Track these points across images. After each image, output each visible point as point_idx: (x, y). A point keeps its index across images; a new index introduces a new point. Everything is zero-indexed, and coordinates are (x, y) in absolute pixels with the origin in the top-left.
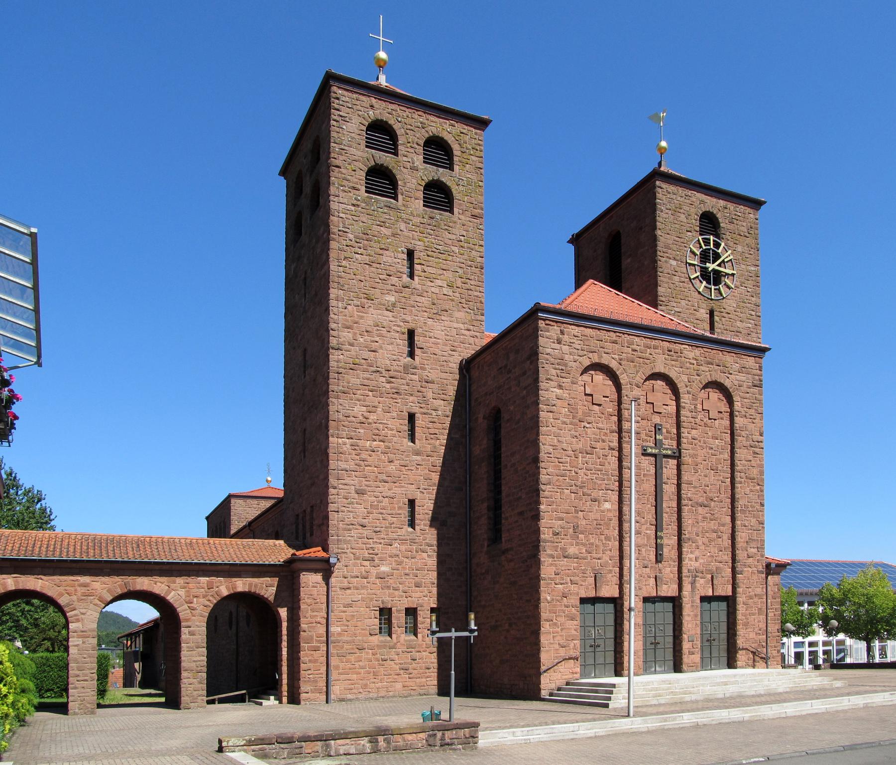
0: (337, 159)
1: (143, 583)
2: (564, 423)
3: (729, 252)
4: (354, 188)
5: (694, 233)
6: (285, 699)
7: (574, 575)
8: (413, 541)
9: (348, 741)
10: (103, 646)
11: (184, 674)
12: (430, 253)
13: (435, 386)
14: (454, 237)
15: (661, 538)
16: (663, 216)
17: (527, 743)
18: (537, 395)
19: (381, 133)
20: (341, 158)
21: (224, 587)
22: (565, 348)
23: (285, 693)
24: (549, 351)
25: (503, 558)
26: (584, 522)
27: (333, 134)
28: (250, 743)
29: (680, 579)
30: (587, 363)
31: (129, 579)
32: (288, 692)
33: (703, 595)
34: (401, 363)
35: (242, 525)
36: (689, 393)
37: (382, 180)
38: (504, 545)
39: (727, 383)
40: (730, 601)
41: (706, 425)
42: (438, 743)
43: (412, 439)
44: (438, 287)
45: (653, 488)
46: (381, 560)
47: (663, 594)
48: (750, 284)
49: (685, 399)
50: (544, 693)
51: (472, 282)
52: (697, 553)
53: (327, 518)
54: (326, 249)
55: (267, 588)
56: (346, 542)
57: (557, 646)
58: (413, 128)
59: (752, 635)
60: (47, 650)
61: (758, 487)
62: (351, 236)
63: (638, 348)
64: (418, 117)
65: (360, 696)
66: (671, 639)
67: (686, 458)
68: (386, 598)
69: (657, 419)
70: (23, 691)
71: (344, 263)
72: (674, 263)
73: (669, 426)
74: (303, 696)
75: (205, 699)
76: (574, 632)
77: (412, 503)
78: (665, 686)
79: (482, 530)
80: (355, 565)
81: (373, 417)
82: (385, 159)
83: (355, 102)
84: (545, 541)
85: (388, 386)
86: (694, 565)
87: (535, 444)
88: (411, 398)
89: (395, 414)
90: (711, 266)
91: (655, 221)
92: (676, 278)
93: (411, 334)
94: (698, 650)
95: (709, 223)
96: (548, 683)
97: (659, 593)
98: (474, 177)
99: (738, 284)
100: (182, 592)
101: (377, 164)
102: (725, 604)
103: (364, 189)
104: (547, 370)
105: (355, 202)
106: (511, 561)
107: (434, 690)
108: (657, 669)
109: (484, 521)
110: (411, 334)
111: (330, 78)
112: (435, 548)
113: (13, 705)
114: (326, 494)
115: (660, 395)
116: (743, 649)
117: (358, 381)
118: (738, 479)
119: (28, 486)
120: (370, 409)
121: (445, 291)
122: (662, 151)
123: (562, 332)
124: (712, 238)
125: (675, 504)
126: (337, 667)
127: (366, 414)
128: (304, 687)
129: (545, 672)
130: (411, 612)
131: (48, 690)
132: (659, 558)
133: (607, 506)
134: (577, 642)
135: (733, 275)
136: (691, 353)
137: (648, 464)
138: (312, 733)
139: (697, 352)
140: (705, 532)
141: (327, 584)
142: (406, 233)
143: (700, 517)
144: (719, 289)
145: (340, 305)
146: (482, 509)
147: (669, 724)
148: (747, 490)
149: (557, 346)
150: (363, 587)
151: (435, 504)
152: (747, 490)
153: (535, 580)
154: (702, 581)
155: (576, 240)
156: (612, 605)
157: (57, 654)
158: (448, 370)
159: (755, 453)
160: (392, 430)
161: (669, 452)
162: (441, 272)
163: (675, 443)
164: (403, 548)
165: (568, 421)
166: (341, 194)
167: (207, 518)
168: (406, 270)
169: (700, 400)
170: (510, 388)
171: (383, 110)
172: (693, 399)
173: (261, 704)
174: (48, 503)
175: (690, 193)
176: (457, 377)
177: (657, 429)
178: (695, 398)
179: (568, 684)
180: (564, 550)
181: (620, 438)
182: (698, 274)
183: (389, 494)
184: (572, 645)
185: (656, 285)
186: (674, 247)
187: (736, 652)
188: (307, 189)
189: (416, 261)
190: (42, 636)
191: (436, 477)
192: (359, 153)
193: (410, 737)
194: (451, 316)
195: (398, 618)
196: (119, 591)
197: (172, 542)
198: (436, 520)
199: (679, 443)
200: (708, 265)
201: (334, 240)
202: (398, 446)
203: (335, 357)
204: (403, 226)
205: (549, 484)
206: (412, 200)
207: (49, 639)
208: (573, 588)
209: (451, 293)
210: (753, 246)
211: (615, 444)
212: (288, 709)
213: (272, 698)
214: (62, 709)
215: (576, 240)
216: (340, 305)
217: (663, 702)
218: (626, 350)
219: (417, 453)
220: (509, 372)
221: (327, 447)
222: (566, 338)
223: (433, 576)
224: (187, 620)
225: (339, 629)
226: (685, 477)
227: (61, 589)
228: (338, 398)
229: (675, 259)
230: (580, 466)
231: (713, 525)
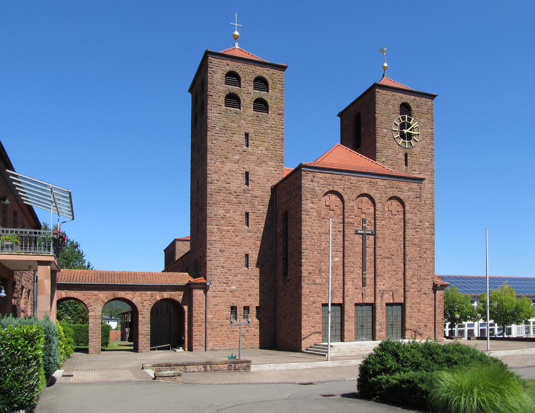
0: (211, 91)
1: (122, 294)
2: (315, 220)
3: (416, 123)
4: (219, 105)
5: (397, 114)
6: (186, 349)
8: (247, 274)
9: (194, 366)
10: (113, 318)
11: (140, 336)
12: (256, 134)
13: (259, 199)
14: (269, 125)
15: (365, 274)
16: (380, 107)
17: (275, 370)
18: (301, 207)
19: (233, 77)
20: (213, 91)
21: (158, 296)
22: (315, 184)
23: (187, 346)
24: (307, 186)
25: (288, 283)
26: (325, 267)
27: (209, 80)
28: (154, 366)
29: (375, 294)
30: (326, 190)
31: (115, 292)
32: (188, 345)
33: (388, 302)
34: (242, 188)
35: (182, 255)
36: (380, 203)
37: (233, 100)
38: (289, 277)
39: (402, 197)
40: (403, 305)
41: (390, 218)
42: (233, 369)
43: (248, 225)
44: (261, 150)
45: (361, 250)
46: (232, 283)
47: (366, 302)
48: (428, 139)
49: (378, 206)
50: (303, 349)
51: (278, 147)
52: (384, 282)
53: (206, 263)
54: (206, 135)
55: (178, 296)
56: (215, 275)
57: (310, 327)
58: (248, 73)
59: (414, 323)
60: (81, 323)
61: (418, 249)
62: (218, 129)
63: (353, 182)
64: (251, 68)
65: (221, 348)
66: (371, 324)
67: (379, 235)
68: (234, 302)
69: (363, 216)
70: (69, 343)
71: (214, 142)
72: (385, 130)
73: (370, 219)
74: (194, 347)
75: (150, 348)
76: (319, 320)
77: (247, 256)
78: (357, 347)
79: (280, 269)
80: (219, 286)
81: (228, 215)
82: (234, 89)
83: (220, 63)
84: (304, 277)
85: (235, 200)
86: (382, 288)
87: (300, 230)
88: (247, 205)
89: (239, 213)
90: (406, 131)
91: (375, 110)
92: (387, 138)
93: (247, 174)
94: (384, 329)
95: (405, 108)
96: (305, 344)
97: (364, 302)
98: (279, 95)
99: (422, 139)
100: (139, 298)
101: (230, 93)
102: (400, 307)
103: (224, 105)
104: (306, 195)
105: (220, 112)
106: (291, 285)
107: (258, 346)
108: (363, 338)
109: (281, 265)
110: (247, 174)
111: (207, 54)
112: (258, 277)
113: (65, 348)
114: (205, 252)
115: (365, 204)
116: (409, 330)
117: (221, 198)
118: (407, 245)
119: (71, 240)
120: (227, 211)
122: (385, 68)
123: (314, 177)
124: (406, 116)
125: (373, 258)
126: (210, 334)
127: (224, 214)
128: (194, 343)
129: (304, 339)
130: (247, 308)
131: (81, 342)
132: (364, 284)
134: (320, 325)
135: (418, 134)
136: (381, 183)
137: (358, 239)
138: (179, 363)
139: (385, 182)
140: (388, 271)
141: (206, 295)
142: (244, 125)
143: (386, 264)
144: (410, 143)
145: (212, 162)
146: (280, 258)
147: (344, 365)
148: (412, 250)
149: (311, 183)
150: (223, 296)
151: (258, 256)
152: (412, 250)
153: (300, 295)
154: (387, 296)
155: (341, 115)
156: (340, 307)
157: (85, 325)
158: (265, 190)
159: (416, 231)
160: (237, 221)
161: (370, 232)
162: (262, 143)
163: (373, 228)
164: (243, 277)
165: (316, 219)
166: (213, 109)
167: (165, 251)
168: (244, 143)
169: (386, 206)
170: (291, 202)
171: (233, 66)
172: (383, 206)
173: (175, 351)
174: (81, 248)
175: (394, 93)
176: (270, 194)
177: (364, 221)
178: (384, 205)
179: (315, 345)
180: (314, 281)
181: (344, 226)
182: (399, 135)
183: (236, 252)
184: (318, 326)
185: (375, 142)
186: (385, 122)
187: (405, 331)
188: (199, 103)
189: (249, 138)
190: (78, 316)
191: (259, 243)
192: (222, 88)
193: (220, 366)
194: (267, 164)
195: (240, 311)
196: (111, 298)
197: (135, 274)
198: (258, 264)
199: (375, 228)
200: (404, 130)
201: (209, 131)
202: (240, 229)
203: (210, 187)
204: (243, 122)
205: (307, 249)
206: (248, 108)
207: (82, 317)
209: (267, 153)
210: (430, 118)
211: (341, 229)
212: (187, 354)
213: (181, 348)
214: (86, 351)
215: (341, 115)
216: (212, 162)
217: (354, 354)
218: (347, 183)
219: (250, 232)
220: (291, 194)
221: (206, 230)
222: (316, 179)
223: (257, 291)
224: (142, 311)
225: (211, 316)
226: (378, 244)
227: (85, 297)
228: (211, 206)
229: (386, 128)
230: (323, 240)
231: (394, 268)
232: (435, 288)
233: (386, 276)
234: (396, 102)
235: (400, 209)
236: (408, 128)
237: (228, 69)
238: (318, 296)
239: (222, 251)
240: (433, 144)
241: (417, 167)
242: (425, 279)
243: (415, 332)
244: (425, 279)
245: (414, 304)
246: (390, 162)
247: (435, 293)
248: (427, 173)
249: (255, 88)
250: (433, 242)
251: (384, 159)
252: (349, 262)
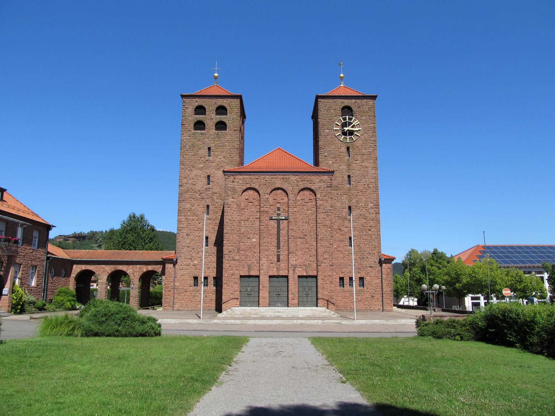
5: (338, 117)
7: (237, 267)
21: (145, 269)
39: (313, 188)
41: (303, 205)
46: (195, 259)
48: (370, 133)
52: (296, 258)
55: (158, 268)
56: (182, 253)
59: (327, 293)
69: (279, 205)
72: (328, 131)
81: (193, 208)
84: (225, 254)
90: (346, 129)
93: (209, 176)
95: (347, 110)
100: (131, 270)
110: (209, 176)
121: (222, 160)
123: (234, 179)
126: (177, 298)
132: (278, 260)
133: (254, 240)
134: (238, 293)
136: (293, 178)
137: (273, 224)
149: (232, 183)
161: (283, 218)
177: (279, 209)
204: (206, 140)
208: (237, 272)
222: (236, 180)
232: (381, 263)
233: (298, 253)
234: (337, 107)
235: (313, 197)
236: (349, 126)
237: (197, 104)
238: (237, 270)
239: (188, 235)
240: (375, 136)
241: (359, 157)
242: (370, 254)
243: (328, 301)
244: (370, 254)
245: (326, 276)
246: (332, 156)
247: (381, 266)
248: (369, 161)
249: (217, 114)
250: (378, 221)
251: (326, 154)
252: (264, 243)
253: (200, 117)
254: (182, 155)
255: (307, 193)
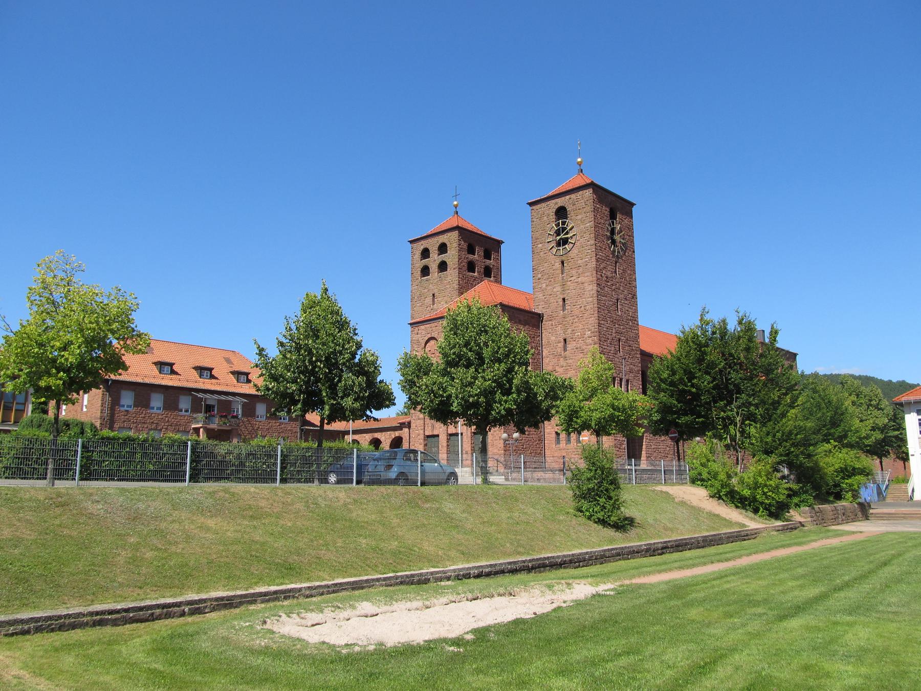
72: (540, 245)
241: (574, 272)
251: (540, 276)
253: (425, 261)
254: (412, 309)
255: (432, 342)
